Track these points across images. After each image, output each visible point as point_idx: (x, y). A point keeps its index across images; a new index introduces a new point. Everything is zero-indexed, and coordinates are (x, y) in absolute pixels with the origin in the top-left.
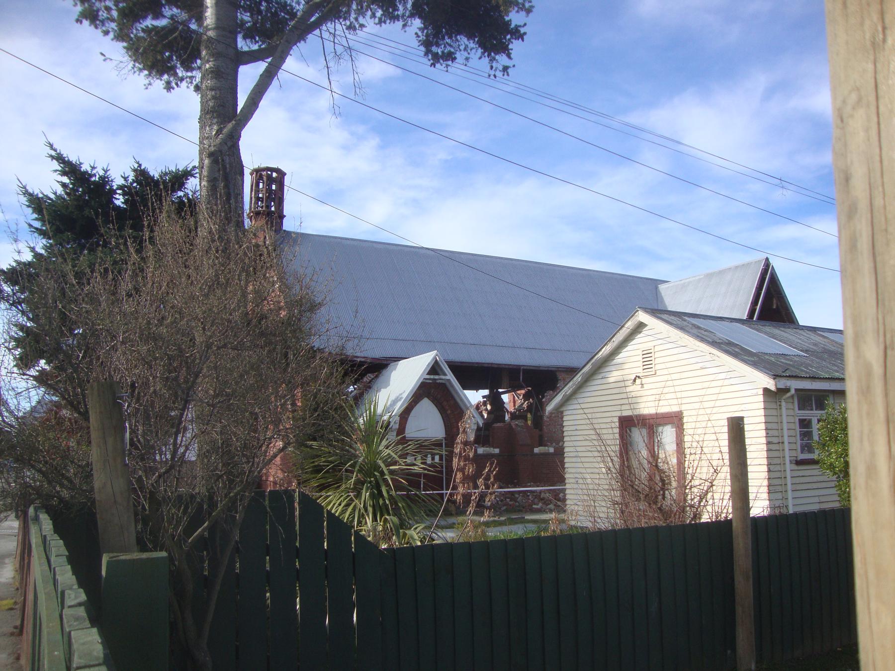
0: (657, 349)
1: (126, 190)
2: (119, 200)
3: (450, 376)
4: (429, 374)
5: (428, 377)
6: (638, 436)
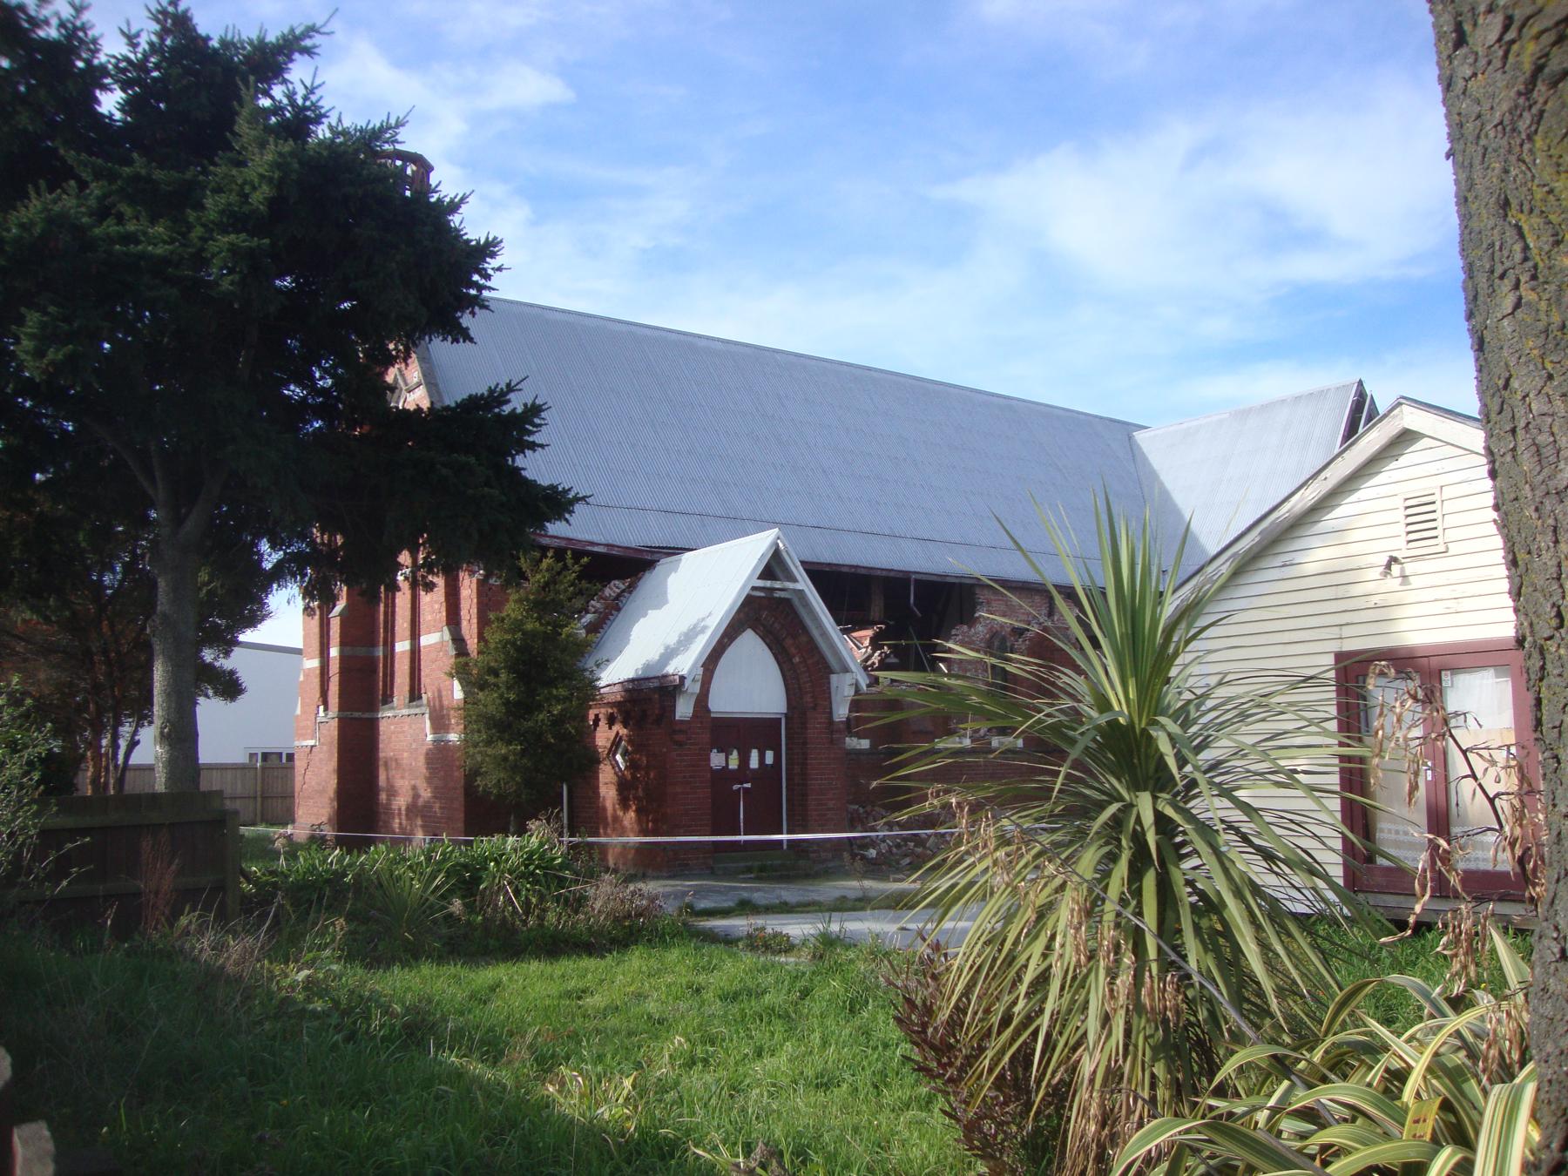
0: (1447, 492)
1: (131, 75)
2: (110, 102)
3: (804, 584)
4: (761, 577)
5: (761, 583)
6: (1389, 697)
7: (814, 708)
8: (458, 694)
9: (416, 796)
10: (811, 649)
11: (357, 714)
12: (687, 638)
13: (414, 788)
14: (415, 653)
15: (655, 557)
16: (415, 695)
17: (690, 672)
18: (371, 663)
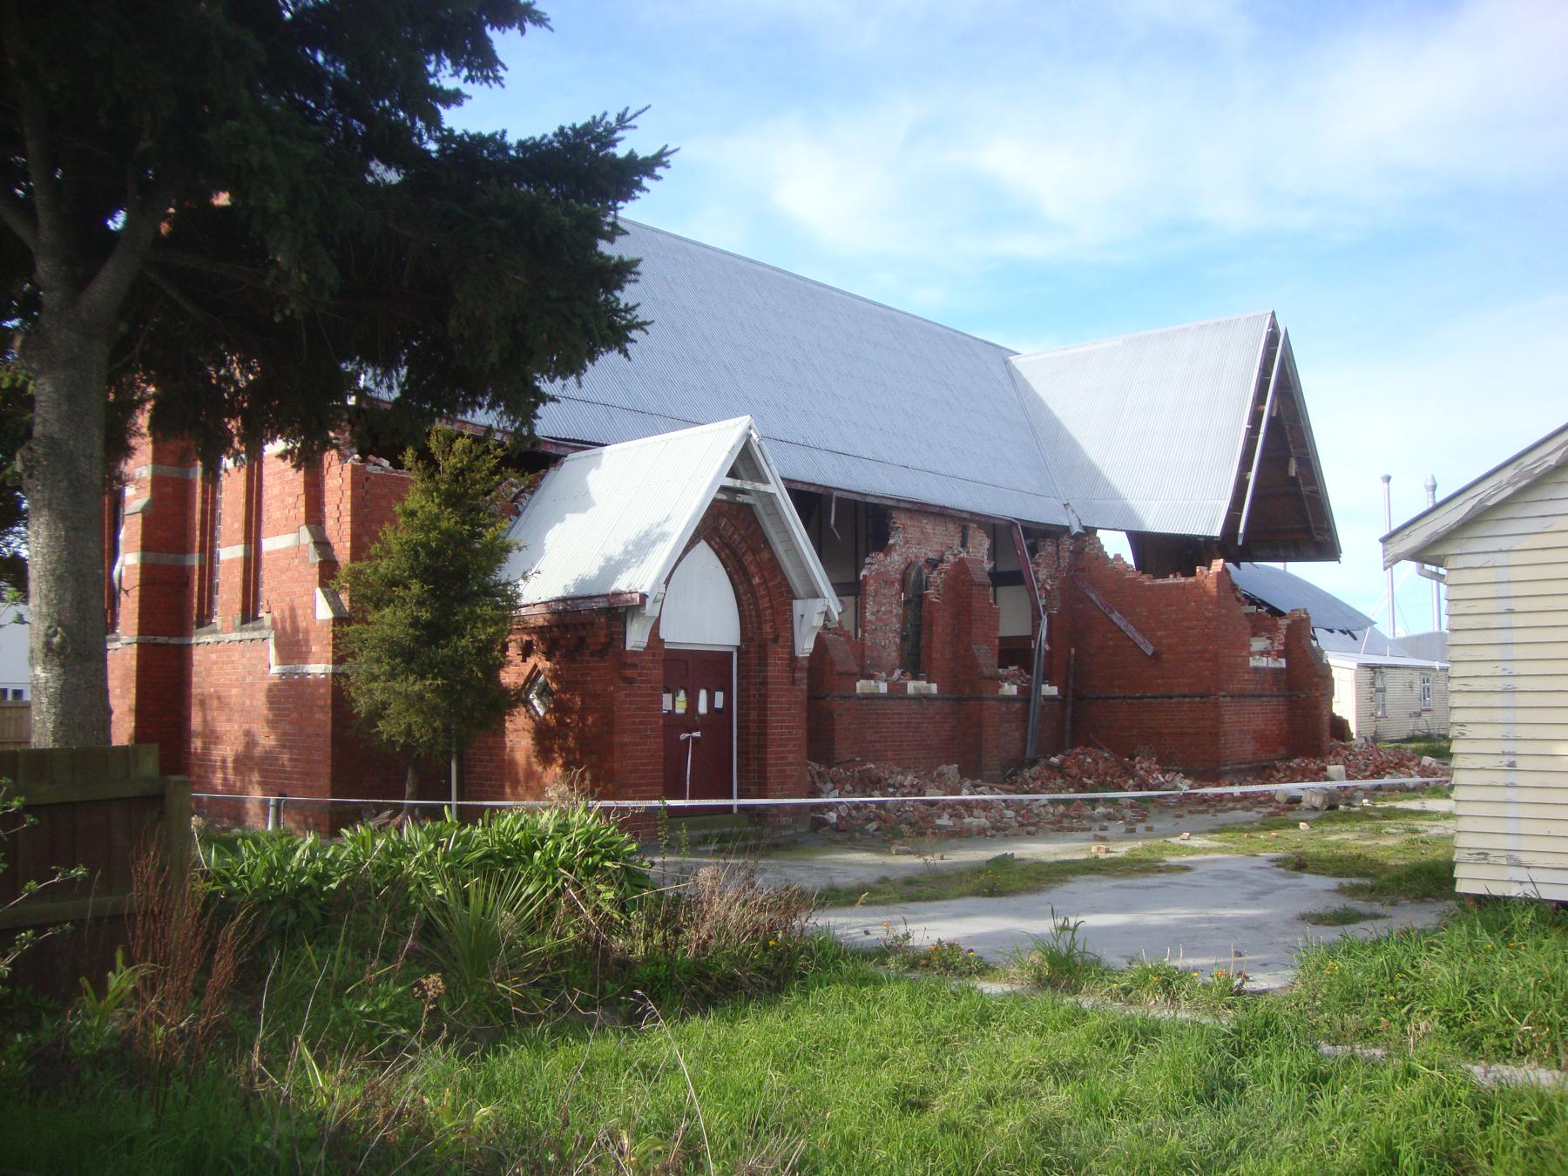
4: (732, 474)
5: (730, 482)
7: (776, 640)
8: (324, 612)
9: (251, 742)
10: (773, 567)
11: (162, 639)
12: (640, 547)
13: (248, 733)
14: (252, 564)
15: (561, 451)
16: (249, 614)
17: (652, 590)
18: (183, 575)
